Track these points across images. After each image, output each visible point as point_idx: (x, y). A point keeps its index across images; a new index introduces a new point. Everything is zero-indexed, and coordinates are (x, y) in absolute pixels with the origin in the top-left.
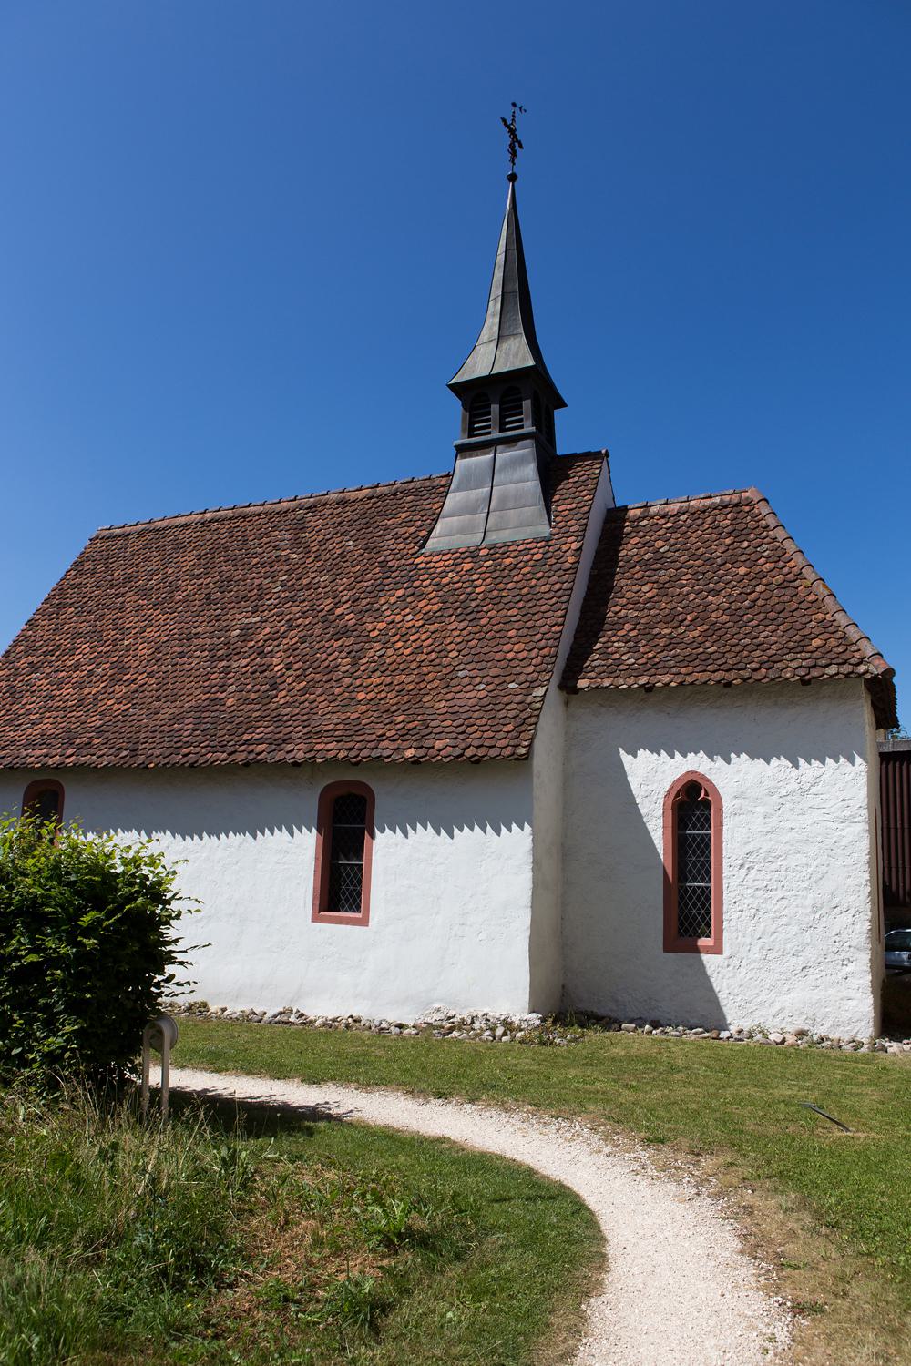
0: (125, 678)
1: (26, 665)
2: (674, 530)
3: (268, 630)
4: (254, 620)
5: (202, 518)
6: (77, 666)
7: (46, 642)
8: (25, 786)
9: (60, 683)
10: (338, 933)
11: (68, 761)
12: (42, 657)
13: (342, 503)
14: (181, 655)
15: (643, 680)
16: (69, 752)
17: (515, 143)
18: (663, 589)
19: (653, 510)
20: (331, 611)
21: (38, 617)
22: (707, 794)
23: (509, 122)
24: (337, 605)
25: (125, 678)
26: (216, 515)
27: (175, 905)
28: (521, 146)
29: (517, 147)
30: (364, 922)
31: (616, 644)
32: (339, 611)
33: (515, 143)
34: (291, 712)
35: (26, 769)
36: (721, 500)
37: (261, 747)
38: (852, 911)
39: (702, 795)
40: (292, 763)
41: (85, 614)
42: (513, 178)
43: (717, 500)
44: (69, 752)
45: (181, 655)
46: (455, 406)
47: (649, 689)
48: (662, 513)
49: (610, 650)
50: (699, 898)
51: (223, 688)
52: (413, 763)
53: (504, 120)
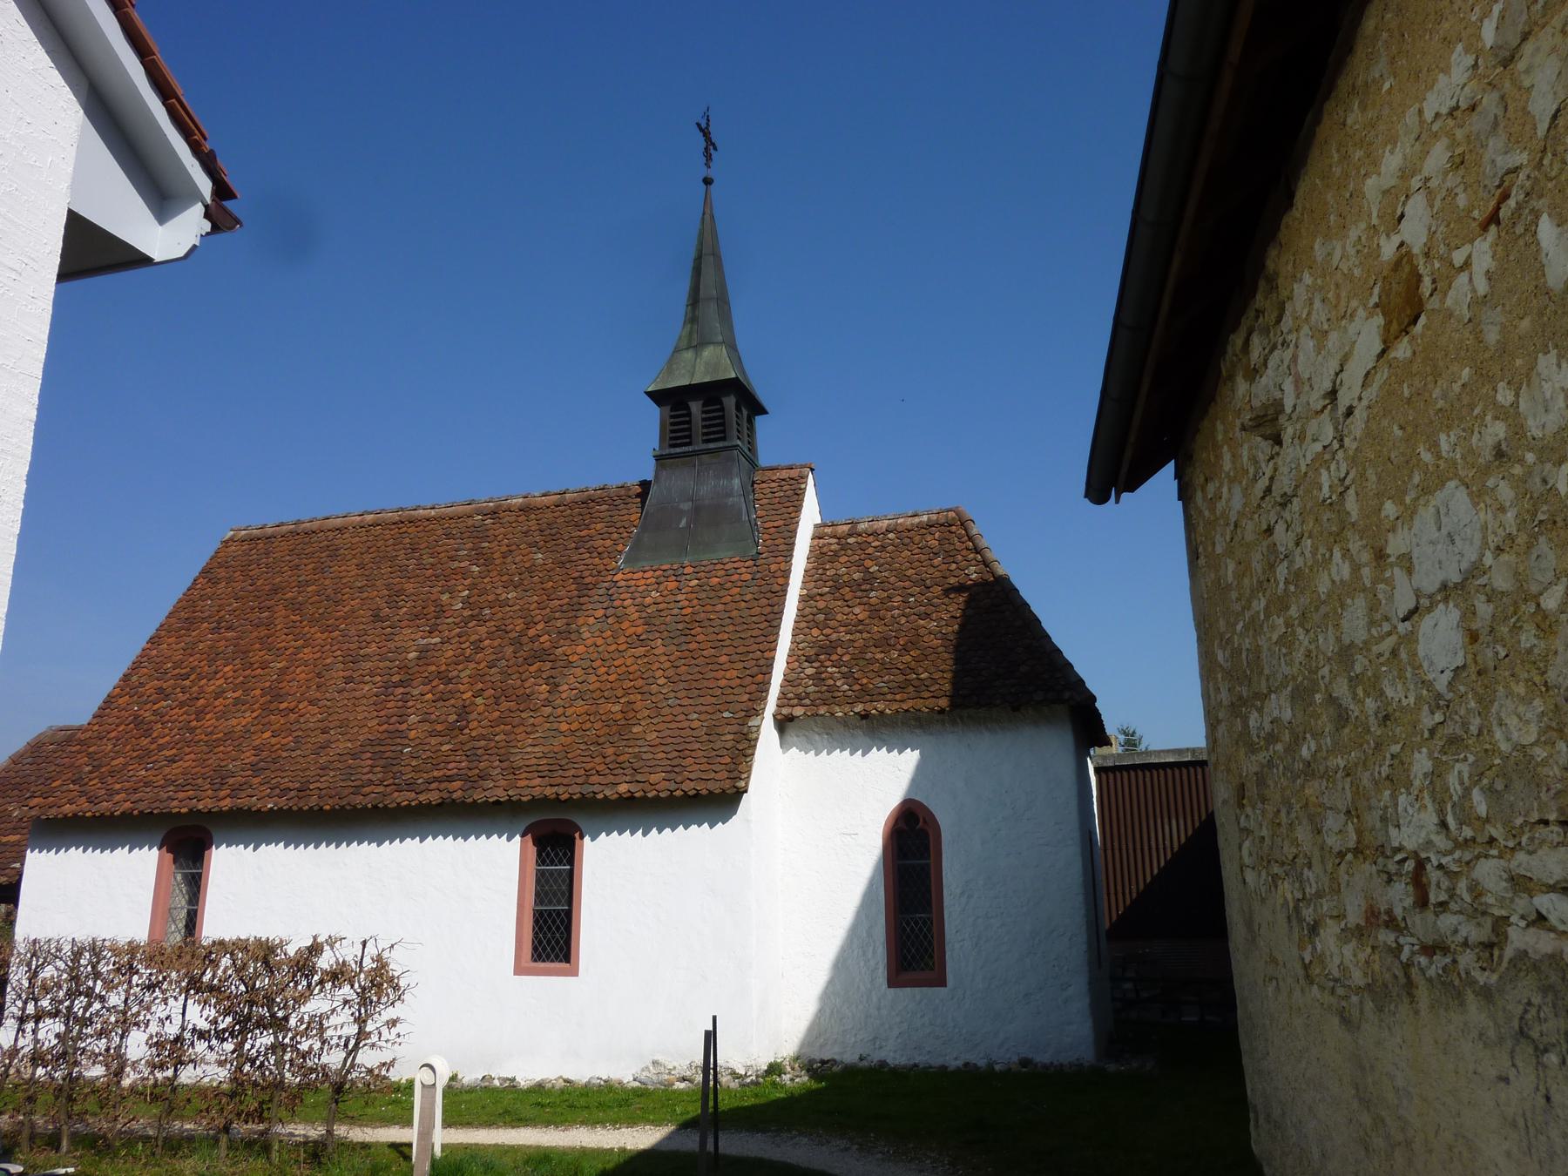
0: (283, 706)
1: (152, 690)
2: (883, 548)
3: (451, 653)
4: (434, 641)
5: (362, 521)
6: (219, 694)
7: (177, 665)
8: (165, 832)
9: (200, 714)
10: (548, 986)
11: (222, 803)
12: (172, 681)
13: (525, 510)
14: (349, 680)
15: (859, 708)
16: (222, 794)
17: (710, 146)
18: (875, 613)
19: (862, 527)
20: (522, 634)
21: (163, 633)
22: (925, 822)
23: (704, 125)
24: (528, 626)
25: (283, 706)
26: (378, 518)
27: (368, 964)
28: (715, 149)
29: (712, 151)
30: (575, 973)
31: (829, 669)
32: (531, 632)
33: (710, 146)
34: (487, 745)
35: (166, 816)
36: (929, 518)
37: (458, 784)
38: (1252, 790)
39: (921, 824)
40: (493, 802)
41: (223, 630)
42: (708, 181)
43: (925, 518)
44: (222, 794)
45: (349, 680)
46: (652, 416)
47: (865, 716)
48: (870, 531)
49: (823, 676)
50: (544, 949)
51: (402, 718)
52: (628, 798)
53: (698, 125)
